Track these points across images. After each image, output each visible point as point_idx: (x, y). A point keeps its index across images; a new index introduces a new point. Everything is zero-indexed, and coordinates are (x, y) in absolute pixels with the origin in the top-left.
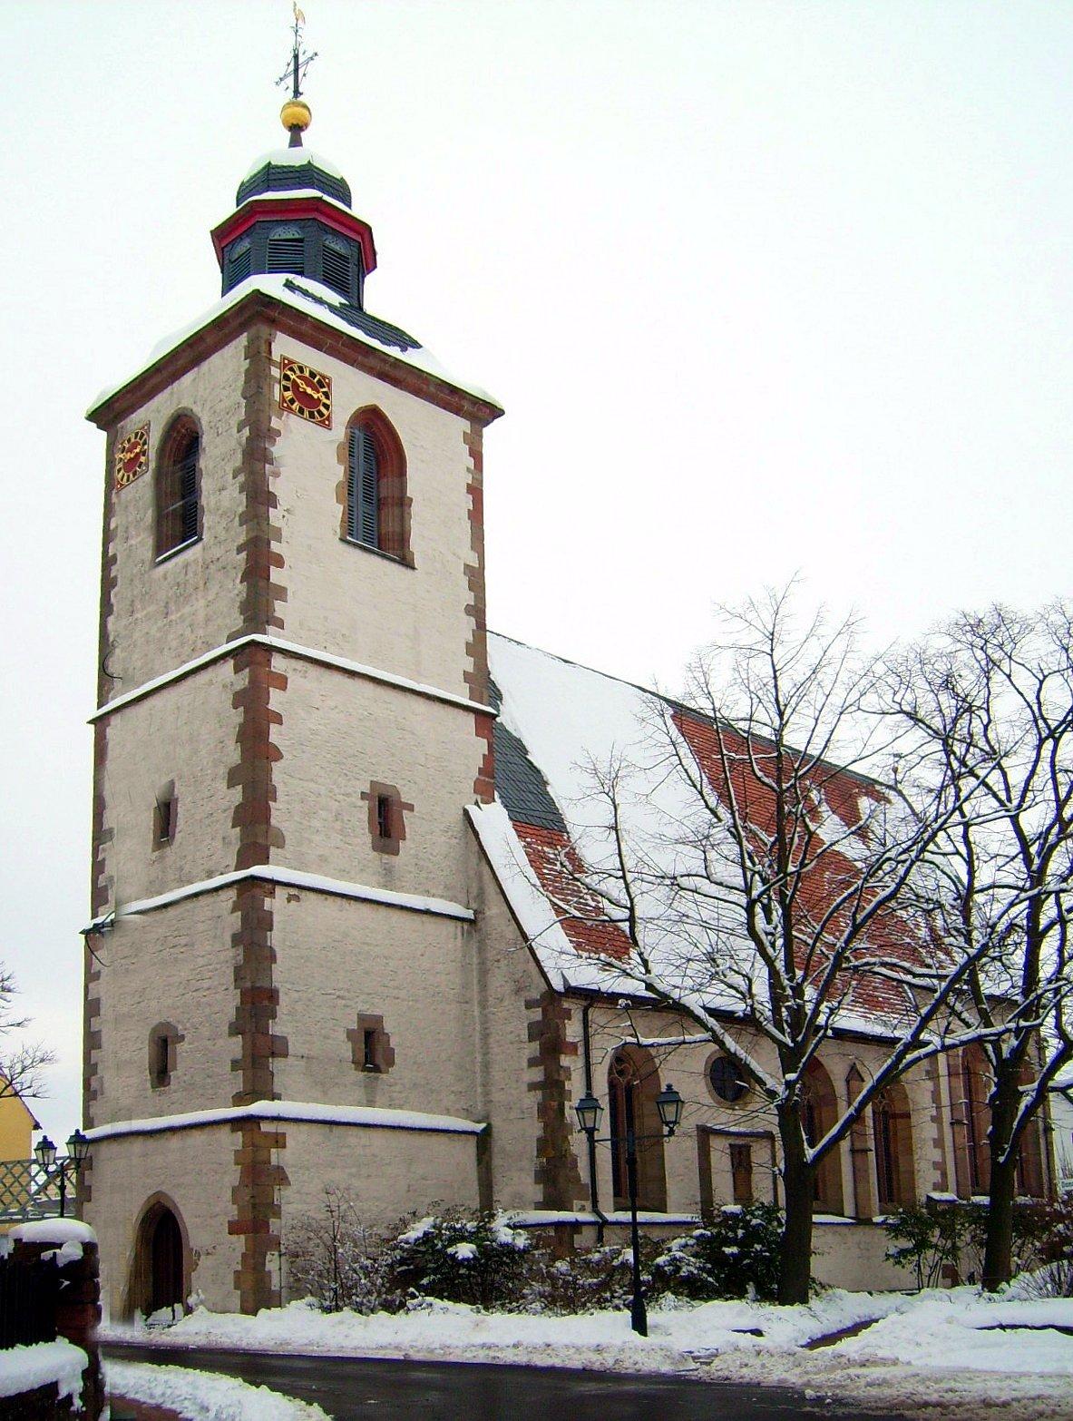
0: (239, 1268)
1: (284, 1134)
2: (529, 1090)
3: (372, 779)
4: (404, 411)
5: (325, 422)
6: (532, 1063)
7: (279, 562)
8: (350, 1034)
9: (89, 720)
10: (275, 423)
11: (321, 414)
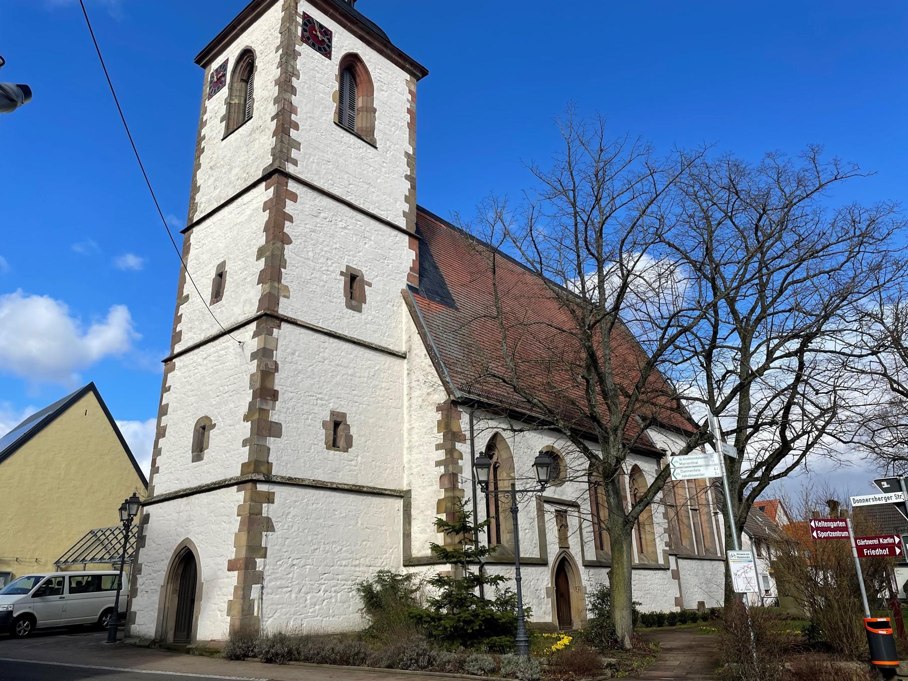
0: (231, 598)
1: (274, 493)
2: (436, 466)
3: (347, 264)
4: (371, 58)
5: (327, 53)
6: (438, 447)
7: (296, 127)
8: (324, 424)
9: (181, 230)
10: (297, 48)
11: (326, 50)
